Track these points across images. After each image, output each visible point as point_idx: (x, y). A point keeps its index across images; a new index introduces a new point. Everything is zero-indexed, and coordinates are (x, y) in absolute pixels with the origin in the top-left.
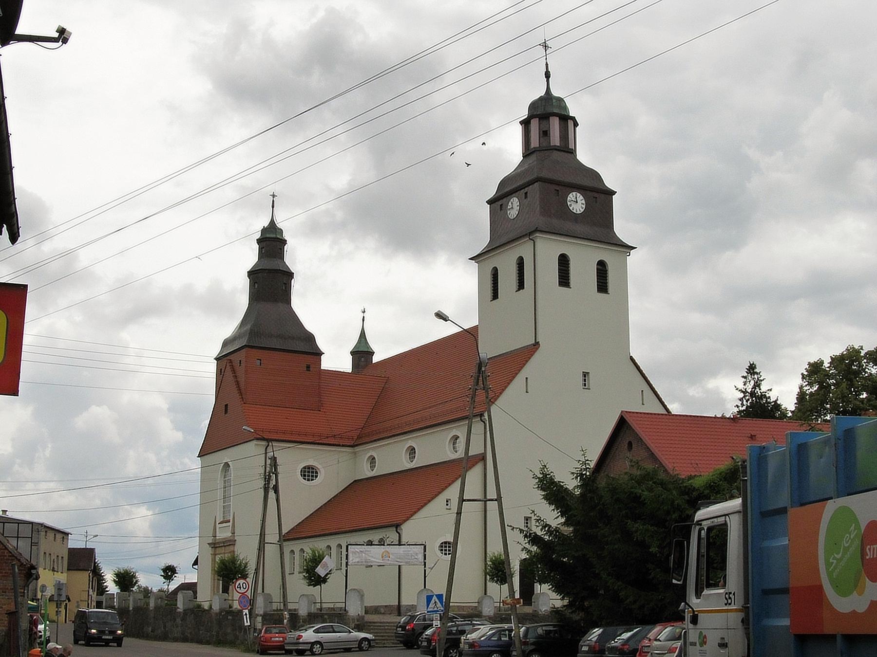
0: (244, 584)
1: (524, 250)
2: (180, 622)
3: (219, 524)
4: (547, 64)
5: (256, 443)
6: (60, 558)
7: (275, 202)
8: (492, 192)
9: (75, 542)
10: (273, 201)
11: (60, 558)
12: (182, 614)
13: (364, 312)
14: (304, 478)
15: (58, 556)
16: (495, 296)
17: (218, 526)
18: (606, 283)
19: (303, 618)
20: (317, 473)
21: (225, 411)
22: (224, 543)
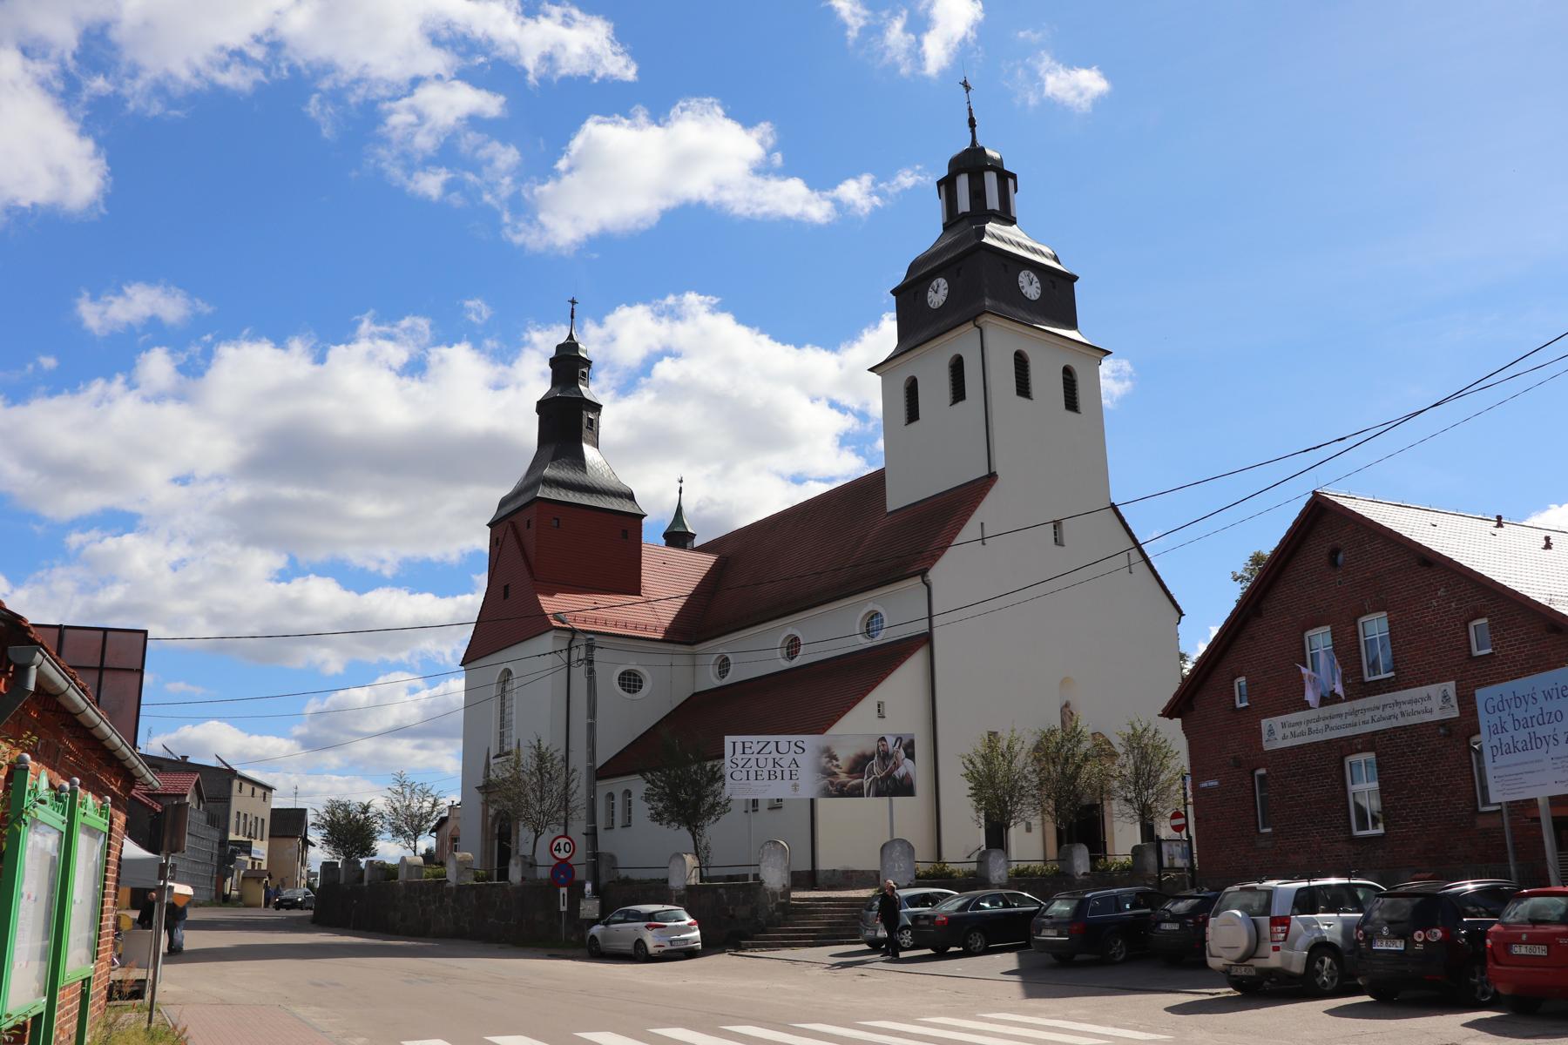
0: (567, 845)
1: (962, 342)
2: (452, 904)
4: (970, 109)
6: (260, 821)
8: (899, 277)
9: (279, 802)
10: (573, 309)
11: (260, 821)
12: (454, 891)
13: (681, 481)
15: (256, 818)
16: (913, 415)
17: (492, 762)
18: (1075, 398)
19: (678, 894)
20: (641, 681)
21: (505, 595)
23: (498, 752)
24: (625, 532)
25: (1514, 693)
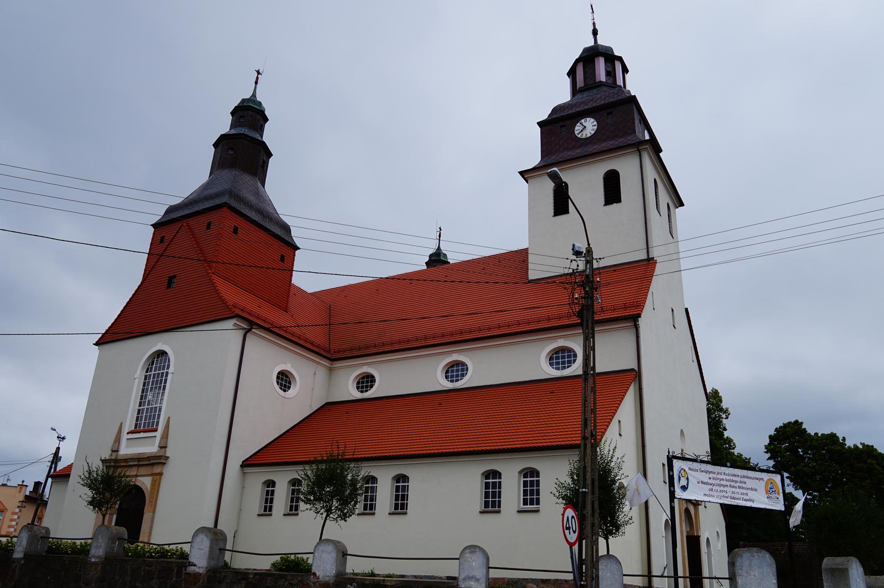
3: (128, 433)
4: (594, 24)
5: (237, 322)
7: (259, 79)
10: (257, 78)
14: (280, 388)
20: (290, 383)
22: (115, 463)
23: (133, 429)
24: (282, 258)
25: (315, 519)
